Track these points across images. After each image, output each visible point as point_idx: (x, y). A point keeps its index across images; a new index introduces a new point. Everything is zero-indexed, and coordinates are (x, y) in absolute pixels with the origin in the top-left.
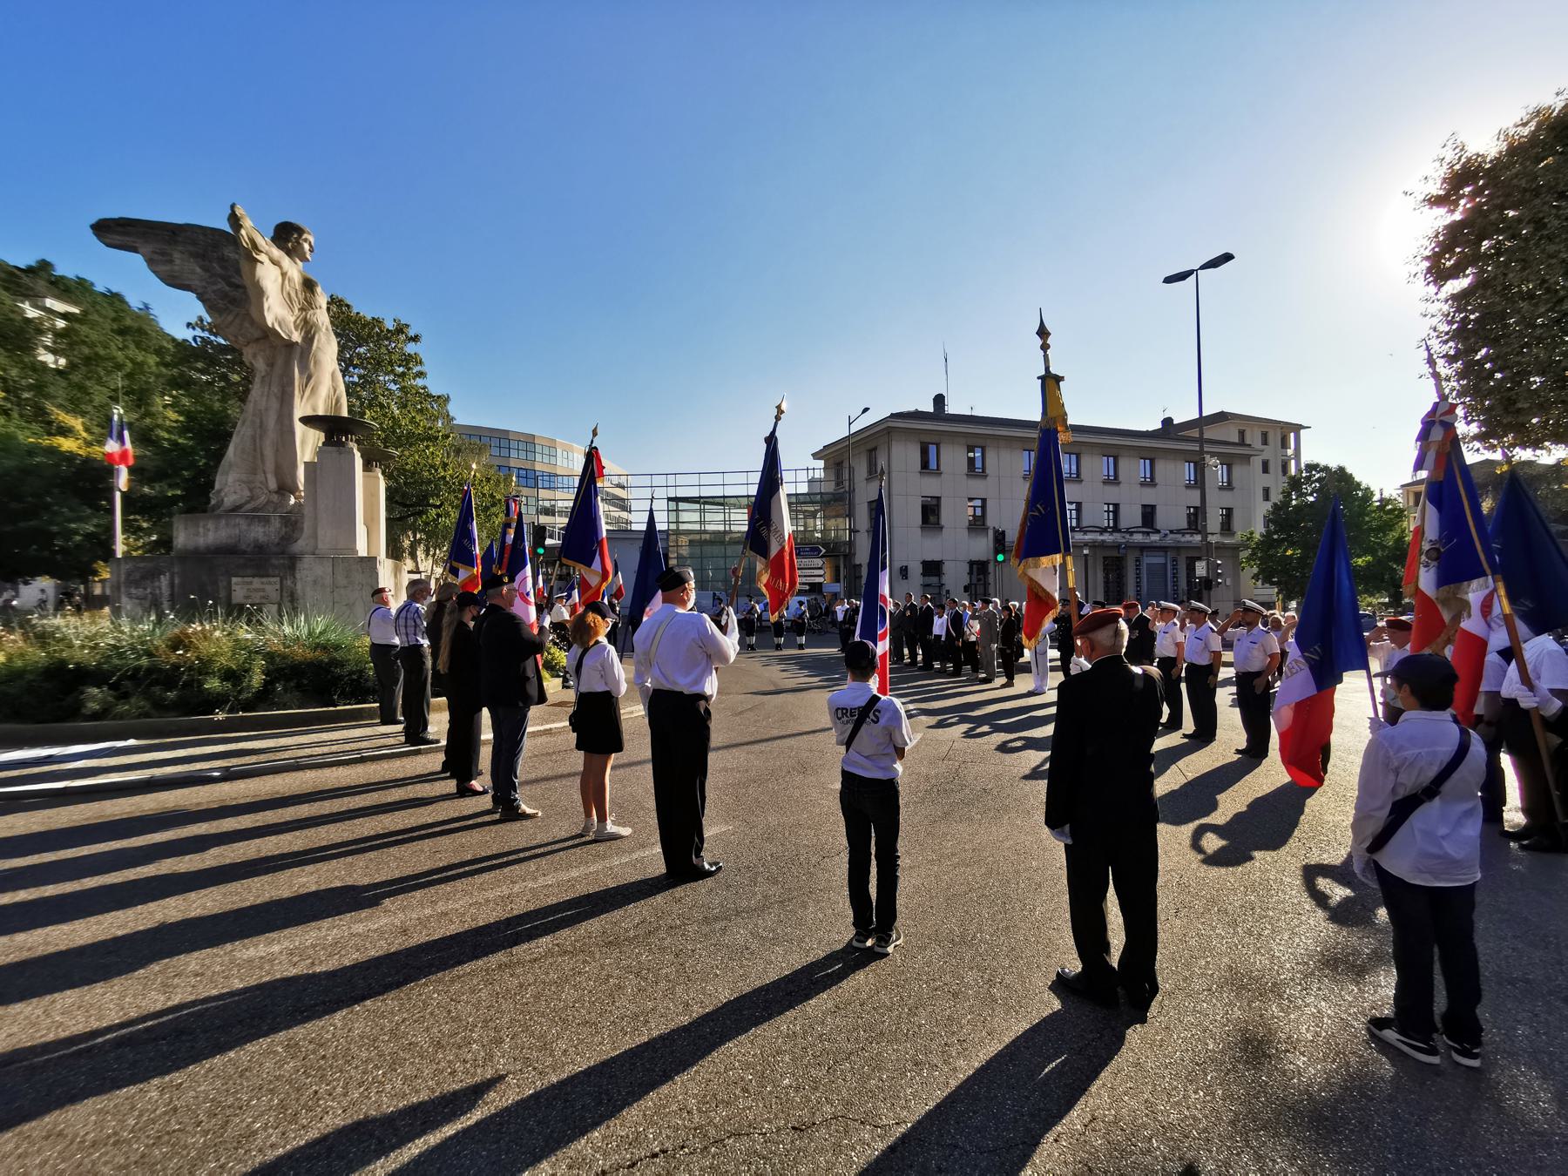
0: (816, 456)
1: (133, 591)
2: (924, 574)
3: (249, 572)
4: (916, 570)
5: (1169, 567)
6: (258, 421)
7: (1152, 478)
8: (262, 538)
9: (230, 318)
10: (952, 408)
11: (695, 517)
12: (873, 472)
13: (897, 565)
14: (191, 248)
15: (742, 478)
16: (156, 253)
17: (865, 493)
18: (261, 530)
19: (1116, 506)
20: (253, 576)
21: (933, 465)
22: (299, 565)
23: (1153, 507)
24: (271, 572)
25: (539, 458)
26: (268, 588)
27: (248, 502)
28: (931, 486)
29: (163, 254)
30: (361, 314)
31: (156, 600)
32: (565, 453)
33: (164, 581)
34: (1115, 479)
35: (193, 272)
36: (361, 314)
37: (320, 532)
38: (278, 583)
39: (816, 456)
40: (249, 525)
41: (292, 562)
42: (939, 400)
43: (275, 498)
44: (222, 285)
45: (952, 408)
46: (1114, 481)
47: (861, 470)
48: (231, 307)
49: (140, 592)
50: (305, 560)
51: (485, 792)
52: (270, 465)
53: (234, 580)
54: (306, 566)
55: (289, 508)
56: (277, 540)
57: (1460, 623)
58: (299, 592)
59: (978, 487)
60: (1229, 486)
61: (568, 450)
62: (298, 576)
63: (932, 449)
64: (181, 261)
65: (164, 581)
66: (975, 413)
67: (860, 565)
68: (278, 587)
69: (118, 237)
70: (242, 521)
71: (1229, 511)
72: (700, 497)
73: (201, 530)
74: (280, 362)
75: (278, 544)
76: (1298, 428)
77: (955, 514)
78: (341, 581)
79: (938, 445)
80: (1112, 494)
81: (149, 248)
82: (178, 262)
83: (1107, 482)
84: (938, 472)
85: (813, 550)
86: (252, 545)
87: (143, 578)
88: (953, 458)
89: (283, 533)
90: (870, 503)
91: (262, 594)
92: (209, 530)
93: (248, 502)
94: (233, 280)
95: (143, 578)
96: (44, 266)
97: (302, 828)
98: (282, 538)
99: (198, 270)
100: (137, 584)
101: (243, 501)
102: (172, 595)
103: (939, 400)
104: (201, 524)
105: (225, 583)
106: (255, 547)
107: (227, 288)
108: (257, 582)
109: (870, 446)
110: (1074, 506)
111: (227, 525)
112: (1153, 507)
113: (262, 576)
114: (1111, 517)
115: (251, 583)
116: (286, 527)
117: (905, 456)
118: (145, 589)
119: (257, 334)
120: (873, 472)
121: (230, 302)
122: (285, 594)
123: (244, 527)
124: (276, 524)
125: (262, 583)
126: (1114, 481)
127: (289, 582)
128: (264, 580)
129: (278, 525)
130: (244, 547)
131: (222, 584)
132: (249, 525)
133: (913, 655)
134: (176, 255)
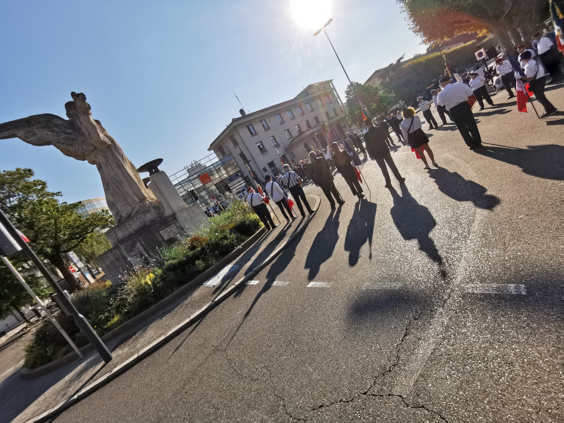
0: (209, 150)
1: (131, 254)
2: (270, 168)
3: (163, 227)
4: (267, 167)
5: (333, 131)
6: (115, 180)
7: (312, 108)
8: (151, 218)
9: (77, 147)
10: (247, 113)
11: (182, 190)
12: (235, 143)
13: (261, 169)
14: (41, 125)
15: (182, 173)
16: (26, 133)
17: (236, 152)
18: (149, 215)
19: (288, 130)
20: (166, 228)
21: (253, 132)
25: (88, 209)
26: (173, 229)
28: (257, 139)
29: (29, 132)
31: (141, 253)
32: (97, 202)
33: (139, 245)
34: (303, 113)
35: (48, 135)
37: (171, 204)
39: (209, 150)
40: (144, 215)
42: (242, 111)
43: (141, 204)
44: (63, 136)
45: (247, 113)
46: (303, 114)
47: (231, 145)
48: (74, 142)
49: (134, 253)
51: (516, 96)
53: (161, 232)
54: (179, 216)
55: (149, 205)
56: (157, 216)
58: (182, 225)
59: (270, 133)
60: (312, 110)
61: (97, 200)
62: (179, 221)
63: (250, 127)
64: (40, 133)
65: (139, 245)
66: (251, 112)
67: (247, 176)
68: (175, 227)
69: (5, 133)
70: (142, 215)
71: (334, 109)
72: (180, 182)
73: (128, 226)
74: (109, 155)
75: (158, 217)
76: (331, 81)
77: (269, 144)
78: (192, 215)
79: (251, 125)
80: (305, 118)
81: (21, 133)
82: (38, 133)
83: (281, 124)
84: (256, 134)
85: (236, 176)
86: (150, 222)
87: (131, 247)
88: (258, 127)
89: (157, 212)
90: (240, 154)
91: (172, 232)
92: (131, 225)
94: (66, 132)
95: (131, 247)
98: (158, 214)
99: (49, 133)
100: (131, 251)
101: (130, 211)
102: (144, 248)
103: (242, 111)
104: (127, 224)
105: (158, 235)
106: (152, 222)
107: (67, 136)
108: (168, 229)
109: (230, 135)
110: (287, 132)
111: (137, 219)
113: (168, 226)
114: (274, 141)
115: (167, 230)
116: (156, 210)
117: (244, 133)
118: (135, 251)
119: (92, 148)
120: (235, 143)
121: (73, 140)
123: (144, 217)
124: (153, 210)
125: (170, 228)
126: (293, 118)
127: (177, 224)
128: (170, 227)
129: (153, 210)
130: (147, 224)
131: (158, 236)
132: (144, 215)
133: (305, 178)
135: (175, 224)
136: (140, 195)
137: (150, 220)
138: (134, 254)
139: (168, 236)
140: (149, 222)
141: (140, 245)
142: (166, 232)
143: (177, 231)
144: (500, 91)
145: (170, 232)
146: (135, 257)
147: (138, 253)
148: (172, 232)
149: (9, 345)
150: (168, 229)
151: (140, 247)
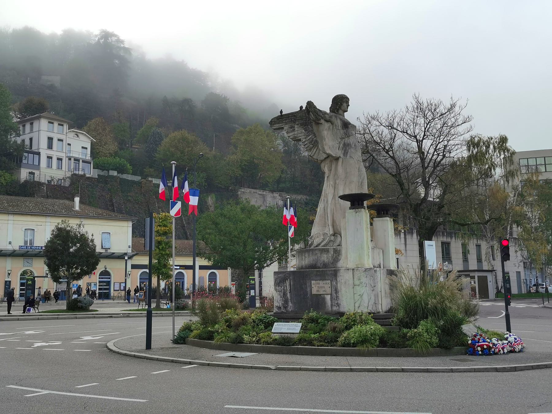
8: (326, 261)
18: (325, 256)
19: (519, 159)
22: (338, 274)
23: (58, 139)
24: (327, 278)
26: (326, 286)
27: (322, 241)
30: (81, 287)
31: (285, 292)
33: (288, 283)
36: (81, 287)
37: (349, 256)
38: (330, 283)
40: (321, 254)
41: (335, 274)
43: (332, 238)
50: (341, 271)
52: (330, 222)
54: (341, 274)
57: (64, 187)
62: (338, 280)
68: (330, 286)
86: (322, 264)
91: (324, 289)
93: (322, 241)
96: (349, 106)
97: (479, 372)
102: (290, 290)
105: (309, 284)
112: (58, 139)
122: (333, 289)
123: (319, 255)
127: (334, 283)
128: (324, 282)
132: (321, 254)
134: (296, 126)
135: (31, 242)
136: (338, 226)
137: (324, 261)
138: (279, 289)
139: (318, 291)
140: (321, 264)
141: (289, 284)
142: (318, 285)
143: (329, 291)
144: (136, 288)
145: (322, 287)
146: (279, 293)
147: (283, 290)
148: (324, 289)
149: (30, 257)
150: (321, 282)
151: (288, 286)
